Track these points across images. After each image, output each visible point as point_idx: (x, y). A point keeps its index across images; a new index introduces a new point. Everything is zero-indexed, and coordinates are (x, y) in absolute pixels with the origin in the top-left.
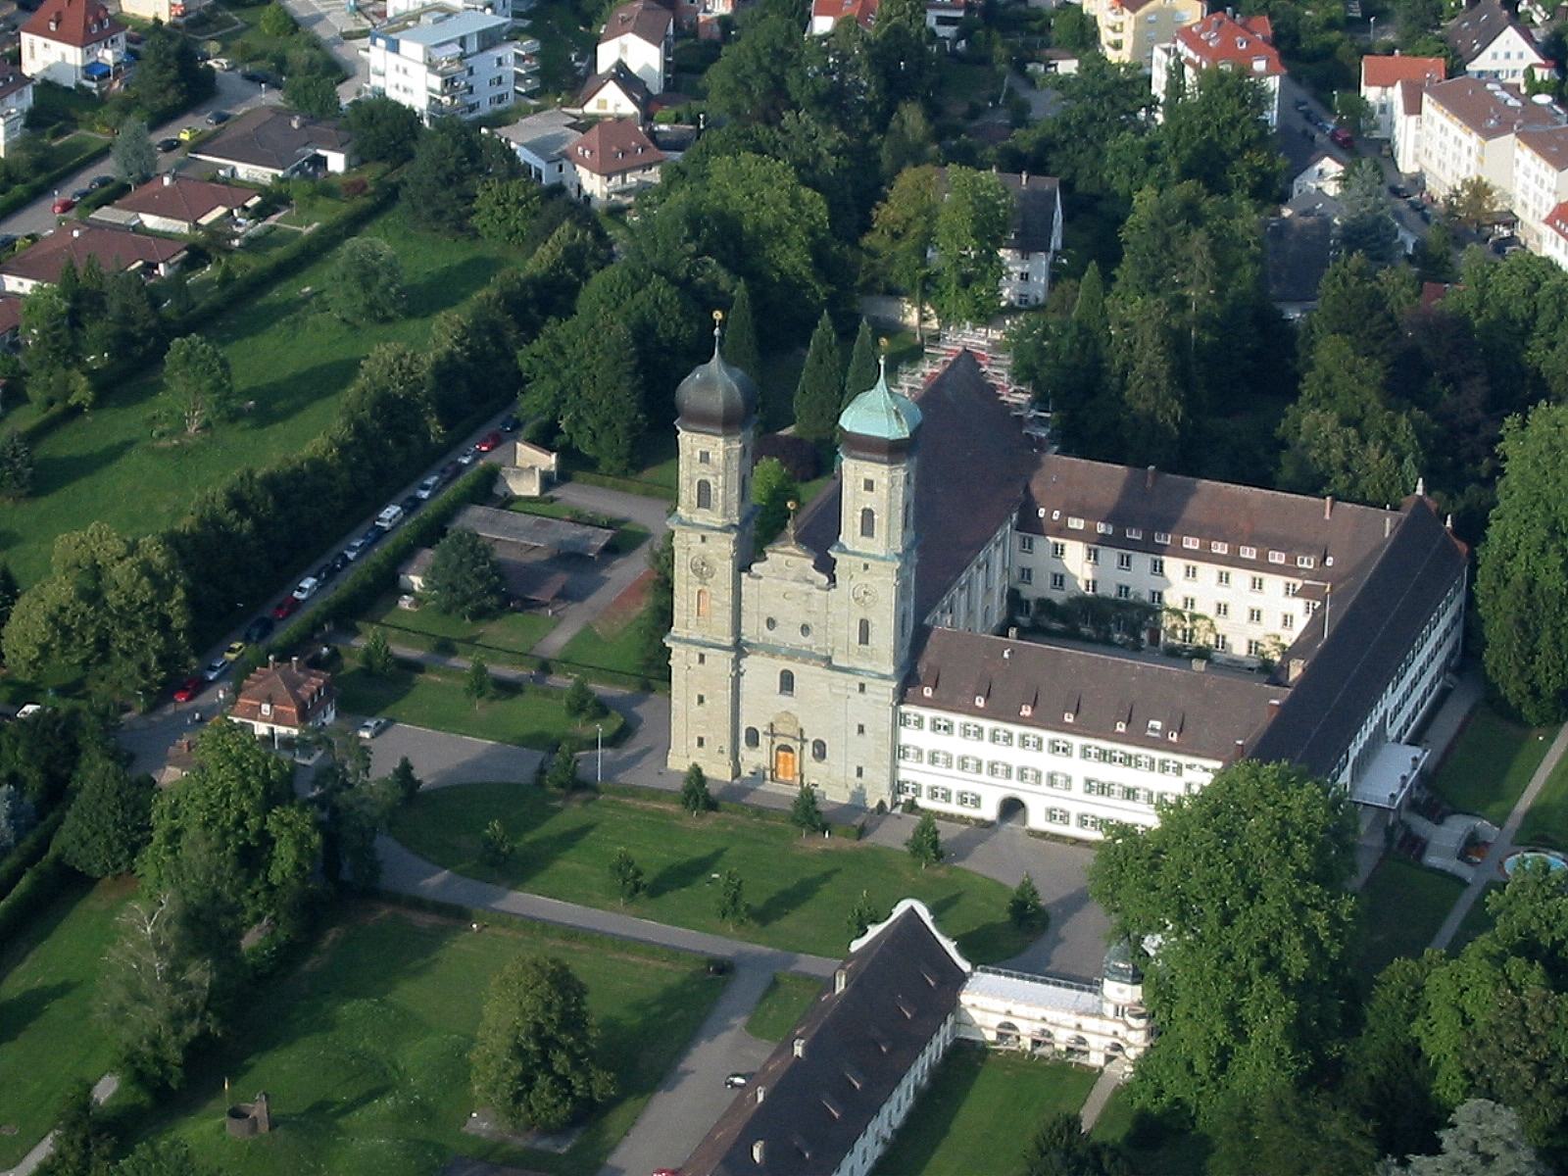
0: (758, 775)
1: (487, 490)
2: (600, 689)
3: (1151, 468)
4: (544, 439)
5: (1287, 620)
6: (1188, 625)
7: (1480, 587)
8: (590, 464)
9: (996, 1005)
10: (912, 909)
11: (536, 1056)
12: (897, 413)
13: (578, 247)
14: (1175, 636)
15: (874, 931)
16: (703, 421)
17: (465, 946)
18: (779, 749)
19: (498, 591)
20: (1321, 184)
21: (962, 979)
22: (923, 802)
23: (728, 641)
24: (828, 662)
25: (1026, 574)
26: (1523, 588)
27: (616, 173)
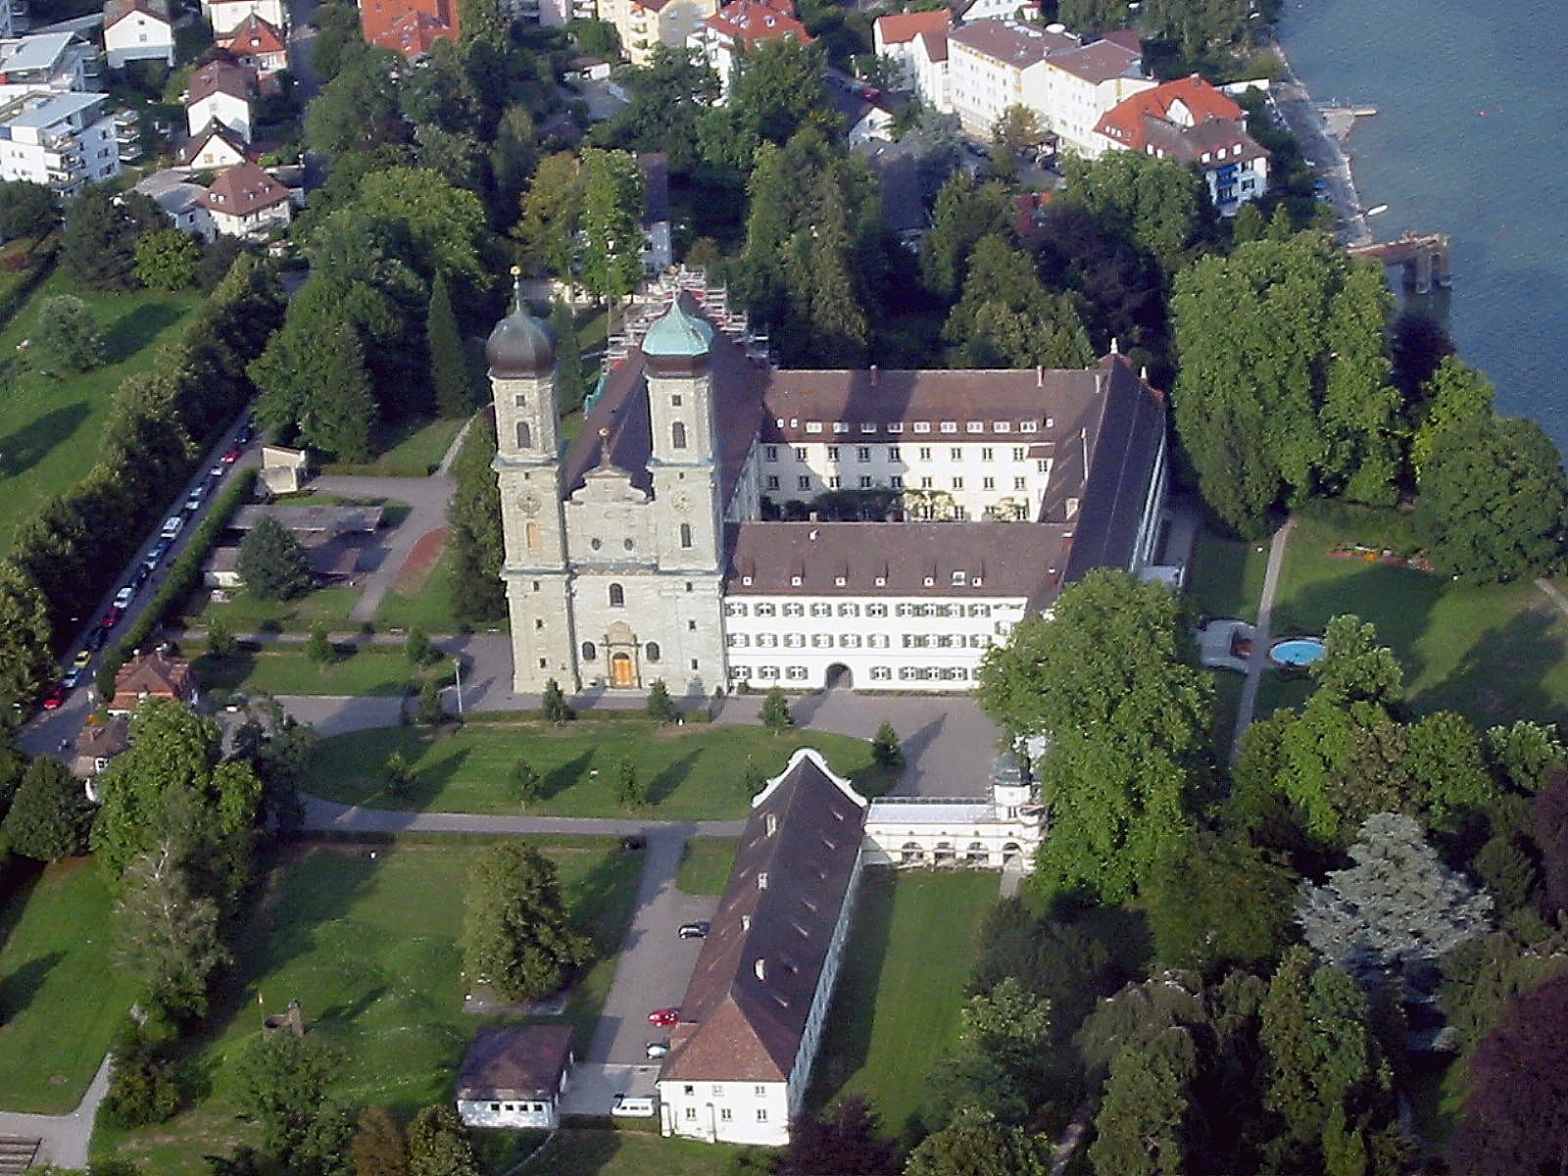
0: (599, 685)
1: (250, 490)
2: (436, 639)
3: (873, 367)
4: (287, 439)
5: (1020, 483)
6: (928, 503)
7: (1183, 426)
8: (331, 458)
9: (896, 830)
10: (807, 757)
11: (522, 937)
12: (694, 331)
13: (257, 273)
14: (917, 515)
15: (773, 785)
16: (514, 368)
17: (399, 866)
18: (614, 658)
19: (298, 572)
20: (873, 134)
21: (860, 814)
22: (755, 682)
23: (561, 566)
24: (655, 569)
25: (774, 482)
26: (1225, 419)
27: (251, 213)
